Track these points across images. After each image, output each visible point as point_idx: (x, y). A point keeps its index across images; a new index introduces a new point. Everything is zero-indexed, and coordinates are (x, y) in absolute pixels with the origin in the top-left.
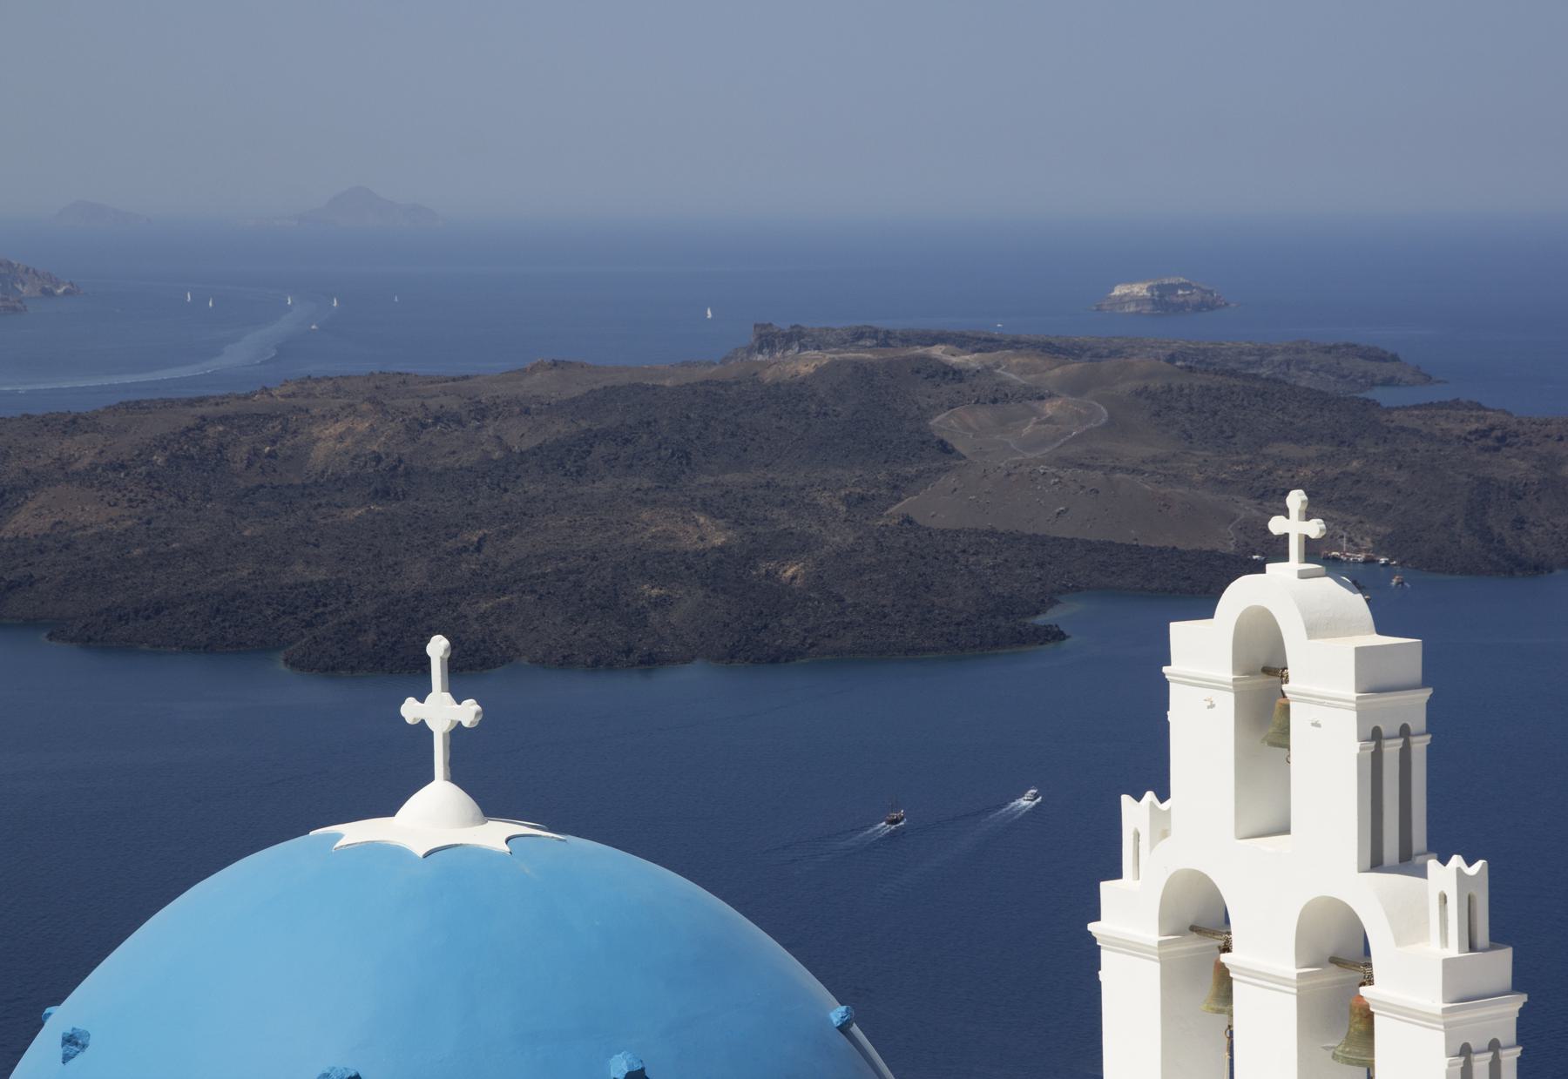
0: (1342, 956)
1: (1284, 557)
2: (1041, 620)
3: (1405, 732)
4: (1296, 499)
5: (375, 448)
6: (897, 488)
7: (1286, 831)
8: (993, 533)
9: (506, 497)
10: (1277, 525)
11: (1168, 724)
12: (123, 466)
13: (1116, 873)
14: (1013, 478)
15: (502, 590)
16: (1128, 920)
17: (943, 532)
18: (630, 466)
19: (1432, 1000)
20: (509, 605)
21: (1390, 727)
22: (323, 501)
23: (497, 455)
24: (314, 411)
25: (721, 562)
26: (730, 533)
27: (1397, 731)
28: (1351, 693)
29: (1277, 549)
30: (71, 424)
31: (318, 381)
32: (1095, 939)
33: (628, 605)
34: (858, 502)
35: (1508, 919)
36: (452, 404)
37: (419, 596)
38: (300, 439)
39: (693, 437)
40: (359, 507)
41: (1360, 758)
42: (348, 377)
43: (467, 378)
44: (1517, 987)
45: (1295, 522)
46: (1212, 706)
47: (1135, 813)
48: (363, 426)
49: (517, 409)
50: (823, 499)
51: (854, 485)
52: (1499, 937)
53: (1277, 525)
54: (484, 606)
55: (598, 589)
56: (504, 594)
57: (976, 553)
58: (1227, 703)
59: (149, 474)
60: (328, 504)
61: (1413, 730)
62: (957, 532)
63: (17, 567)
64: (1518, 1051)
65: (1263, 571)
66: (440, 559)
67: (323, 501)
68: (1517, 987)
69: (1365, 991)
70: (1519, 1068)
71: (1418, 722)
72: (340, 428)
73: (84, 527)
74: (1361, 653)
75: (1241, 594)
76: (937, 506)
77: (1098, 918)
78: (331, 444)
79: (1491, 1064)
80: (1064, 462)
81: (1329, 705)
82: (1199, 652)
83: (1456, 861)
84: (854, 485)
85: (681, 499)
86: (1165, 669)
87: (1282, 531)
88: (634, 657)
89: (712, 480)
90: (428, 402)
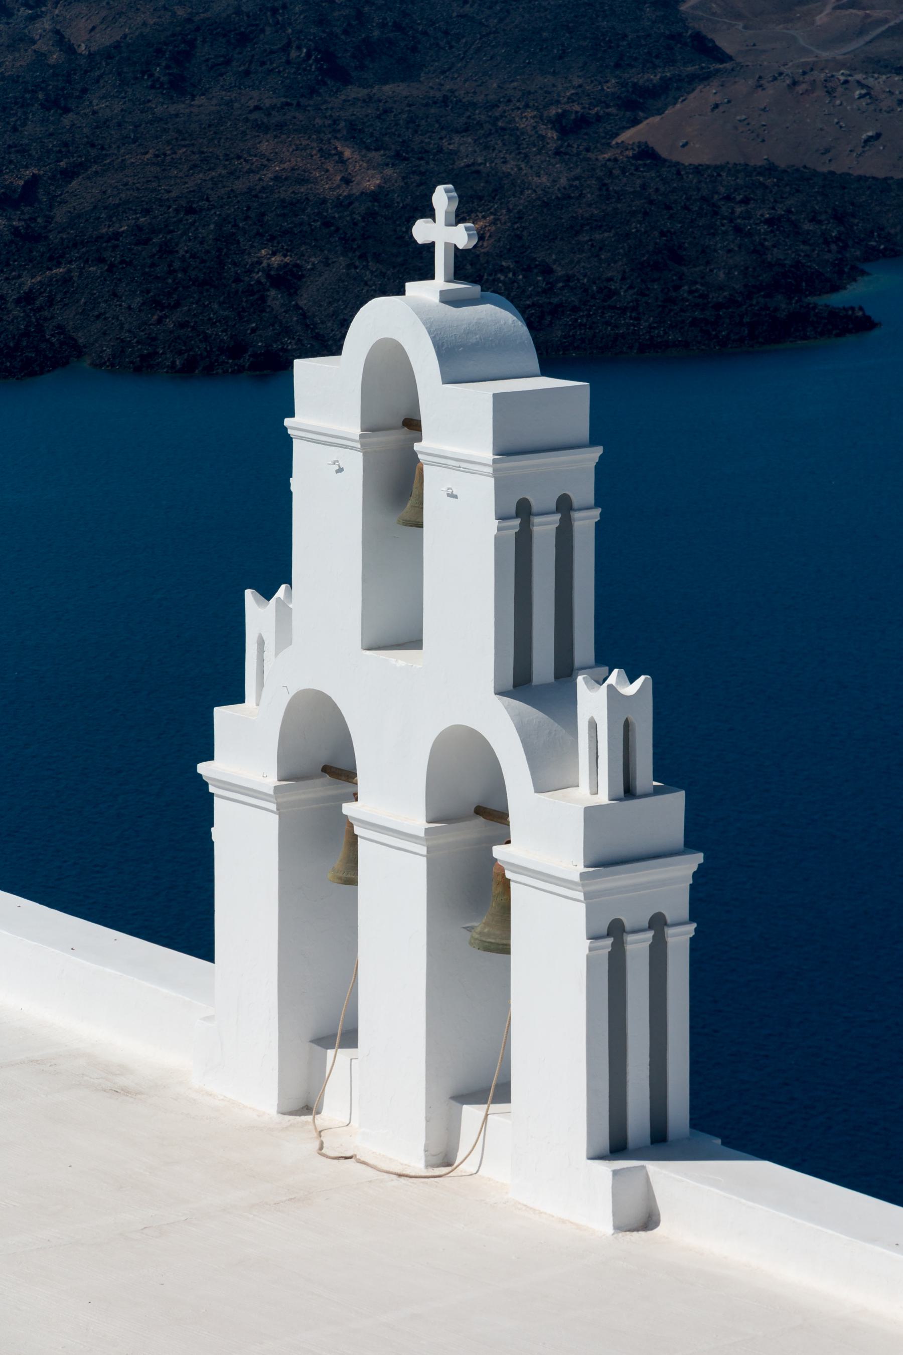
0: (472, 810)
1: (427, 273)
2: (836, 300)
3: (564, 505)
4: (442, 198)
6: (638, 103)
7: (414, 642)
8: (770, 169)
9: (67, 120)
10: (422, 231)
11: (290, 494)
13: (238, 697)
14: (801, 88)
15: (56, 259)
16: (243, 753)
17: (698, 170)
18: (247, 73)
19: (571, 862)
20: (66, 280)
21: (542, 498)
23: (55, 57)
25: (374, 214)
26: (389, 171)
27: (553, 506)
28: (487, 454)
29: (420, 263)
33: (238, 280)
34: (571, 127)
39: (338, 30)
44: (691, 843)
45: (441, 231)
46: (340, 470)
47: (258, 614)
50: (525, 121)
51: (570, 100)
52: (668, 774)
53: (422, 231)
54: (29, 282)
55: (193, 256)
56: (59, 265)
57: (746, 201)
58: (355, 463)
61: (576, 502)
62: (719, 168)
64: (690, 929)
65: (401, 291)
68: (691, 843)
69: (499, 852)
70: (693, 950)
71: (583, 490)
74: (498, 398)
75: (379, 321)
76: (690, 131)
77: (210, 757)
79: (651, 947)
80: (879, 65)
81: (466, 471)
82: (325, 397)
83: (615, 677)
84: (570, 100)
85: (318, 121)
86: (287, 422)
87: (428, 240)
88: (246, 360)
89: (363, 93)
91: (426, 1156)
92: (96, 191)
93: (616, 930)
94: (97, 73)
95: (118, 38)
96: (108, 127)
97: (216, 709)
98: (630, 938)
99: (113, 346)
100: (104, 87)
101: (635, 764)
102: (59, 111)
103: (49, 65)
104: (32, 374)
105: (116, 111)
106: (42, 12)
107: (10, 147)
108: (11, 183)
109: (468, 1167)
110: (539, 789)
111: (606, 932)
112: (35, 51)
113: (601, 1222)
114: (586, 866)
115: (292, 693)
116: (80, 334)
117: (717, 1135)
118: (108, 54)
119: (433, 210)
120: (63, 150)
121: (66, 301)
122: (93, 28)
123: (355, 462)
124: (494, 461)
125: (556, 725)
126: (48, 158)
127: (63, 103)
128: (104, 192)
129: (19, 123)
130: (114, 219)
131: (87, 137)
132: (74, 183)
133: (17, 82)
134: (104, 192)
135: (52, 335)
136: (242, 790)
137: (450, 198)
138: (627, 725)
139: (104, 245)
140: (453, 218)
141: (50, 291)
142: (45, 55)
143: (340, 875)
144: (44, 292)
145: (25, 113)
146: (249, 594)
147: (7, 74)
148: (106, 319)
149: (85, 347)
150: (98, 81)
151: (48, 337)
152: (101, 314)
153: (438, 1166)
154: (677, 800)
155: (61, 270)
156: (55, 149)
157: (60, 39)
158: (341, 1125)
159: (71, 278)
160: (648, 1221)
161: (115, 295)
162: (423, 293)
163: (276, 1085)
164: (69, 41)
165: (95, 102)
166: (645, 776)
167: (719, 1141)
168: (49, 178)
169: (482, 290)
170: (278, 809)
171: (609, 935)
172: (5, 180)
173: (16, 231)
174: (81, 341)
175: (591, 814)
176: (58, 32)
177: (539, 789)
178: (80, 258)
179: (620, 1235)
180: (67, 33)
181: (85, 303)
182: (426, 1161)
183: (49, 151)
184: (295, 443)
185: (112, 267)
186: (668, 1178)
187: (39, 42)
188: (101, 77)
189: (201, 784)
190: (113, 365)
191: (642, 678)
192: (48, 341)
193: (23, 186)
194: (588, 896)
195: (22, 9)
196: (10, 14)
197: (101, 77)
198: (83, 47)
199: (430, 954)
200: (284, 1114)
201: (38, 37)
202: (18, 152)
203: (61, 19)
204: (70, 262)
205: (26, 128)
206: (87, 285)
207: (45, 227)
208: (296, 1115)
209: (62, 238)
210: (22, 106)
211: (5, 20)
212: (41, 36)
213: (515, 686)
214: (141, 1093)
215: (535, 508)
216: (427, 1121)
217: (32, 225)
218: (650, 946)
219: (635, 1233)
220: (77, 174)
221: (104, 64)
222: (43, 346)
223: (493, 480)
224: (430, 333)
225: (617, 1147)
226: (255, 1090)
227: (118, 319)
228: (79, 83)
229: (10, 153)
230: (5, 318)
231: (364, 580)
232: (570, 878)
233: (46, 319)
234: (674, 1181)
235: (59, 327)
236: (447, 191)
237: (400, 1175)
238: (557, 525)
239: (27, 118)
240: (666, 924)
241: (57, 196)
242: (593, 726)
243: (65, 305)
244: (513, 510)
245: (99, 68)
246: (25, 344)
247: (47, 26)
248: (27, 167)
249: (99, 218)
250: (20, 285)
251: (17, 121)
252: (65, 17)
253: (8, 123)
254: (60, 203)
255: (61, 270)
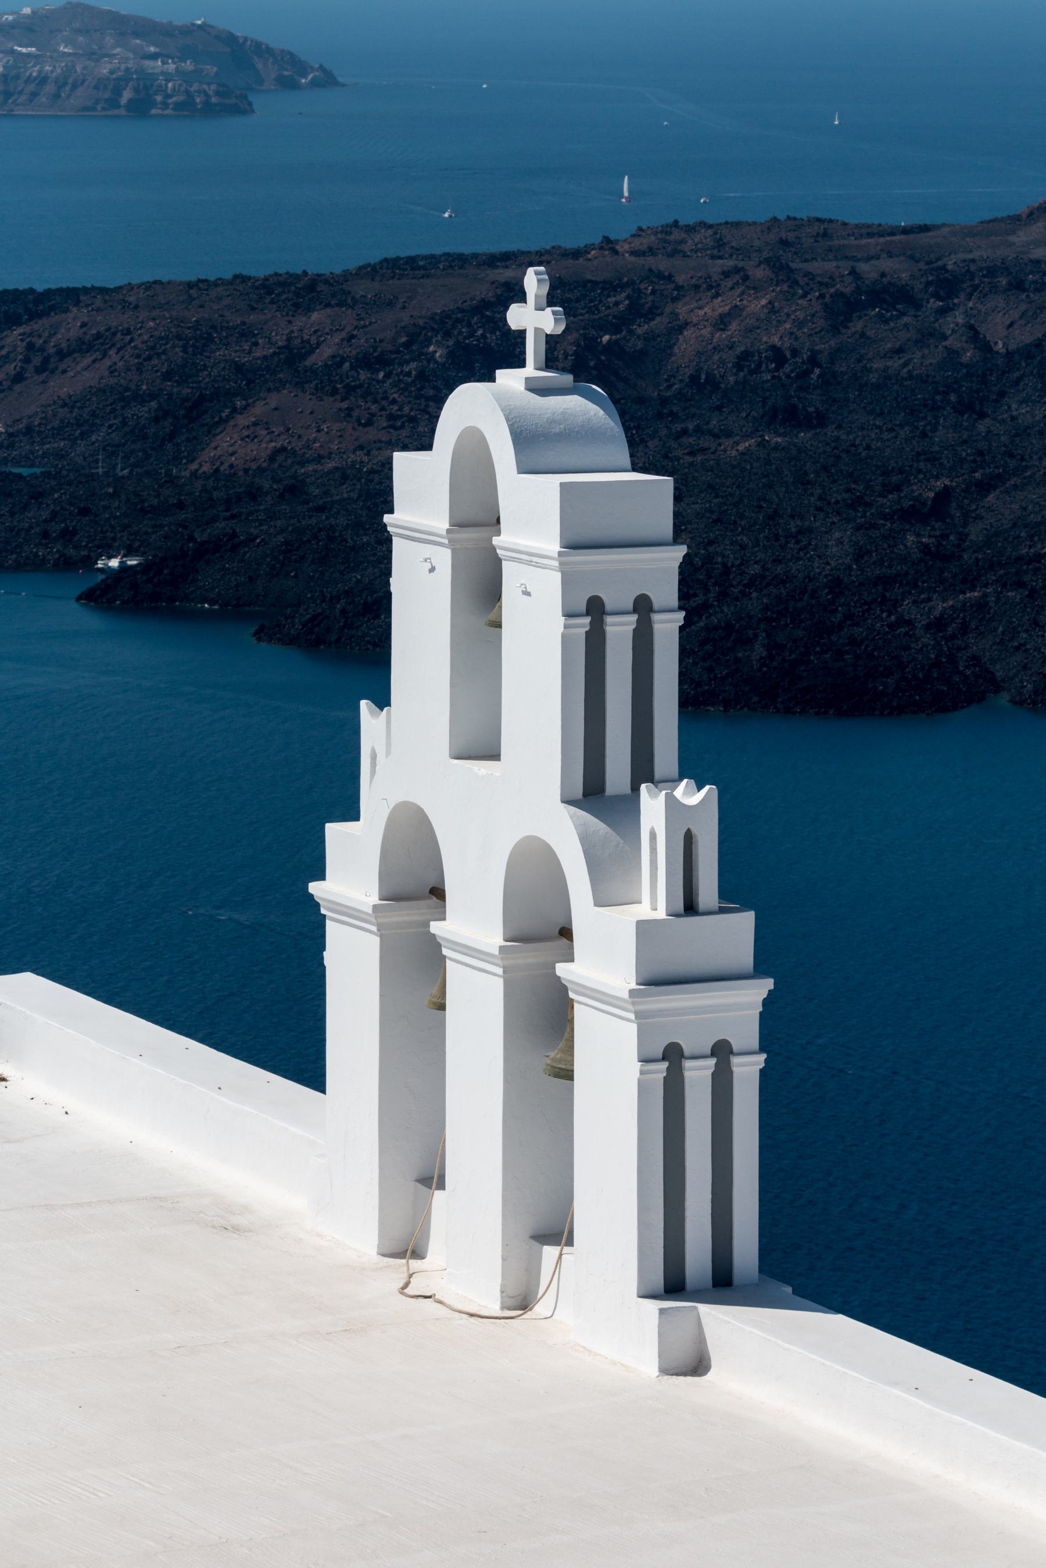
0: (541, 929)
5: (775, 340)
9: (982, 427)
12: (382, 361)
16: (350, 873)
19: (622, 979)
20: (981, 606)
21: (618, 597)
22: (691, 426)
24: (681, 279)
27: (630, 606)
28: (553, 546)
30: (302, 291)
31: (690, 229)
32: (318, 905)
35: (747, 868)
36: (899, 270)
37: (836, 585)
38: (659, 323)
40: (747, 436)
41: (565, 640)
42: (737, 225)
43: (925, 228)
45: (533, 318)
48: (757, 305)
49: (1004, 282)
53: (518, 316)
54: (940, 606)
56: (973, 588)
59: (422, 375)
60: (698, 430)
63: (214, 519)
65: (492, 379)
66: (872, 526)
67: (691, 426)
71: (665, 591)
72: (720, 306)
73: (319, 459)
78: (706, 332)
82: (420, 489)
86: (387, 518)
90: (863, 267)
91: (502, 1297)
92: (1015, 507)
93: (673, 1055)
94: (1016, 374)
95: (1040, 335)
96: (1029, 435)
97: (328, 825)
98: (688, 1064)
99: (1035, 681)
100: (1024, 390)
101: (698, 879)
102: (974, 416)
103: (962, 364)
104: (945, 710)
105: (1038, 418)
106: (954, 304)
107: (918, 454)
108: (921, 494)
109: (541, 1309)
110: (598, 903)
111: (660, 1056)
112: (946, 347)
113: (646, 1362)
114: (637, 984)
115: (391, 807)
116: (998, 667)
117: (786, 1281)
118: (1027, 353)
119: (524, 294)
120: (978, 459)
121: (982, 629)
122: (1012, 324)
123: (443, 558)
124: (560, 554)
125: (618, 838)
126: (961, 468)
127: (978, 407)
128: (1025, 509)
129: (929, 428)
130: (1036, 539)
131: (1005, 446)
132: (991, 498)
133: (926, 382)
134: (1025, 509)
135: (966, 667)
136: (593, 994)
137: (539, 281)
138: (689, 839)
139: (1025, 567)
140: (544, 301)
141: (964, 618)
142: (957, 352)
143: (435, 1000)
144: (957, 618)
145: (936, 418)
146: (363, 703)
147: (915, 373)
148: (1026, 651)
149: (1003, 681)
150: (1017, 383)
151: (961, 669)
152: (1021, 645)
153: (515, 1309)
154: (745, 922)
155: (976, 594)
156: (969, 458)
157: (974, 334)
158: (439, 1268)
159: (987, 603)
160: (697, 1366)
161: (1036, 624)
162: (510, 381)
163: (377, 1224)
164: (985, 337)
165: (1014, 406)
166: (708, 891)
167: (789, 1290)
168: (963, 491)
169: (575, 381)
170: (379, 930)
171: (664, 1059)
172: (913, 491)
173: (925, 549)
174: (999, 675)
175: (644, 928)
176: (972, 327)
177: (598, 903)
178: (997, 581)
179: (666, 1377)
180: (982, 329)
181: (1003, 633)
182: (502, 1303)
183: (962, 461)
184: (396, 541)
185: (1033, 592)
186: (722, 1323)
187: (951, 339)
188: (1020, 379)
189: (312, 904)
190: (1034, 703)
191: (707, 787)
192: (961, 673)
193: (934, 499)
194: (639, 1015)
195: (932, 300)
196: (918, 306)
197: (1020, 379)
198: (1000, 344)
199: (506, 1081)
200: (384, 1255)
201: (950, 332)
202: (927, 460)
203: (974, 312)
204: (986, 586)
205: (937, 434)
206: (1005, 612)
207: (958, 546)
208: (397, 1258)
209: (977, 559)
210: (932, 409)
211: (913, 313)
212: (953, 330)
213: (584, 795)
214: (250, 1231)
215: (609, 606)
216: (504, 1260)
217: (944, 543)
218: (713, 1074)
219: (682, 1378)
220: (995, 488)
221: (1024, 364)
222: (957, 678)
223: (559, 575)
224: (507, 420)
225: (674, 1286)
226: (354, 1232)
227: (1040, 651)
228: (995, 385)
229: (918, 461)
230: (913, 645)
231: (452, 685)
232: (478, 947)
233: (959, 649)
234: (728, 1327)
235: (974, 657)
236: (537, 273)
237: (472, 1315)
238: (634, 626)
239: (938, 423)
240: (732, 1052)
241: (972, 511)
242: (653, 836)
243: (981, 633)
244: (583, 607)
245: (1018, 369)
246: (935, 675)
247: (960, 320)
248: (937, 478)
249: (1019, 537)
250: (930, 610)
251: (925, 426)
252: (980, 311)
253: (917, 428)
254: (975, 518)
255: (976, 594)
